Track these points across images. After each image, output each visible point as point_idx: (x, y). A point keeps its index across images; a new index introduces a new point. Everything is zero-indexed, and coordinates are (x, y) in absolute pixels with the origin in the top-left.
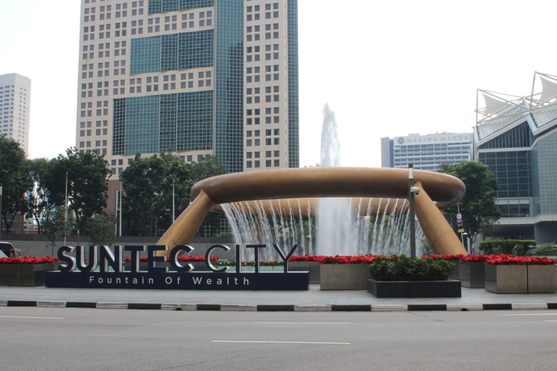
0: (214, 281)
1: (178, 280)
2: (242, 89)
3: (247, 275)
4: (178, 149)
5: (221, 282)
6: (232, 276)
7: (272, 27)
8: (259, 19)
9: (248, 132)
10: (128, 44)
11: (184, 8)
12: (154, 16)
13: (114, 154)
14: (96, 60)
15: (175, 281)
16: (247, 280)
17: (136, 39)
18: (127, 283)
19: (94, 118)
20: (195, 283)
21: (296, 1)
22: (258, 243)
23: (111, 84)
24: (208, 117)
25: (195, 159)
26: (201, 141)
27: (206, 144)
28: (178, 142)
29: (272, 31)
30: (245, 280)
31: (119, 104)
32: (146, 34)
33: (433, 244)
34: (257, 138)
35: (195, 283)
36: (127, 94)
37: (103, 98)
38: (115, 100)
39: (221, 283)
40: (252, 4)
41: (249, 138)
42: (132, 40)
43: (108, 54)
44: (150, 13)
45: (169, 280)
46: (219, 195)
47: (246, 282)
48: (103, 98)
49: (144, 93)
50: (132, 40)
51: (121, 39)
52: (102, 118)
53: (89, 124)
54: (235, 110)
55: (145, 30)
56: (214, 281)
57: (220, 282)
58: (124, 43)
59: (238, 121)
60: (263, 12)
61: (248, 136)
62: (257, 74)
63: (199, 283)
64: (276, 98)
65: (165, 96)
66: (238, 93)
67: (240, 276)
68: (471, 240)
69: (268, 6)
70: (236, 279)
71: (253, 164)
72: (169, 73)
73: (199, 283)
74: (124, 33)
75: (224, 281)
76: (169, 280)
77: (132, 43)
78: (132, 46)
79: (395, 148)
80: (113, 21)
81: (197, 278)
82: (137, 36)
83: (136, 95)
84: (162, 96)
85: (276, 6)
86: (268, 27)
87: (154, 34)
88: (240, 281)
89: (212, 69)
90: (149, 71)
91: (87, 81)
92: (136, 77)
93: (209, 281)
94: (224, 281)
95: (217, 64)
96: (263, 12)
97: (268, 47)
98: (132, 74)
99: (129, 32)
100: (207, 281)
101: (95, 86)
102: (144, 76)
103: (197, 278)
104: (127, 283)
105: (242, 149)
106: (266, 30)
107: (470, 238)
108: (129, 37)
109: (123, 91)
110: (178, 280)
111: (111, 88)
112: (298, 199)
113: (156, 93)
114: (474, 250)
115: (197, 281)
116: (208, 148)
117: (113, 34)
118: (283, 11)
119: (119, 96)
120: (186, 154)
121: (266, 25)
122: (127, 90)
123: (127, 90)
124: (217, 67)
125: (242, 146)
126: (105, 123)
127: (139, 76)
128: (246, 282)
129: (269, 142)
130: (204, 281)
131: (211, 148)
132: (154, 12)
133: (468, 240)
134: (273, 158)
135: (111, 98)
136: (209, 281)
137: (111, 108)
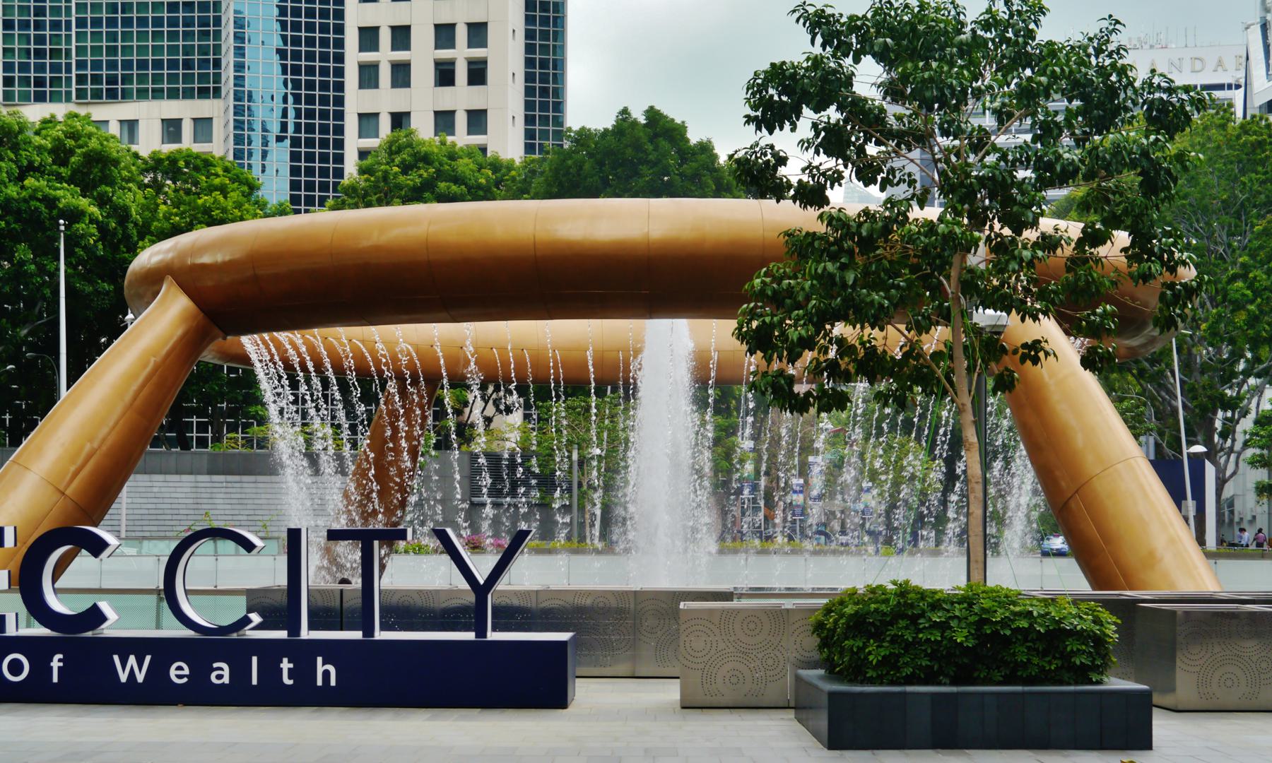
0: (200, 671)
1: (56, 663)
2: (340, 116)
3: (331, 650)
4: (81, 94)
5: (226, 673)
6: (271, 652)
9: (362, 30)
15: (41, 668)
16: (332, 669)
18: (287, 681)
20: (123, 677)
21: (560, 8)
22: (379, 523)
24: (204, 50)
26: (173, 64)
28: (81, 65)
30: (320, 669)
33: (1066, 503)
34: (401, 55)
35: (123, 677)
39: (226, 680)
40: (383, 16)
41: (369, 57)
45: (16, 667)
46: (233, 301)
47: (326, 674)
54: (310, 42)
56: (200, 671)
57: (222, 673)
59: (324, 143)
60: (423, 55)
61: (362, 48)
62: (401, 55)
63: (140, 678)
66: (324, 130)
67: (304, 654)
68: (1220, 472)
69: (444, 34)
70: (286, 665)
71: (385, 74)
73: (140, 678)
75: (240, 672)
76: (16, 667)
81: (132, 660)
85: (478, 32)
88: (304, 671)
93: (178, 672)
94: (240, 672)
96: (423, 55)
100: (173, 672)
103: (132, 660)
104: (287, 681)
105: (340, 101)
107: (1215, 463)
110: (56, 663)
112: (373, 328)
114: (1231, 504)
115: (132, 669)
116: (203, 93)
118: (507, 55)
120: (112, 114)
121: (438, 27)
125: (340, 87)
128: (326, 674)
129: (445, 75)
130: (158, 672)
131: (217, 93)
133: (1210, 471)
134: (461, 53)
136: (178, 672)
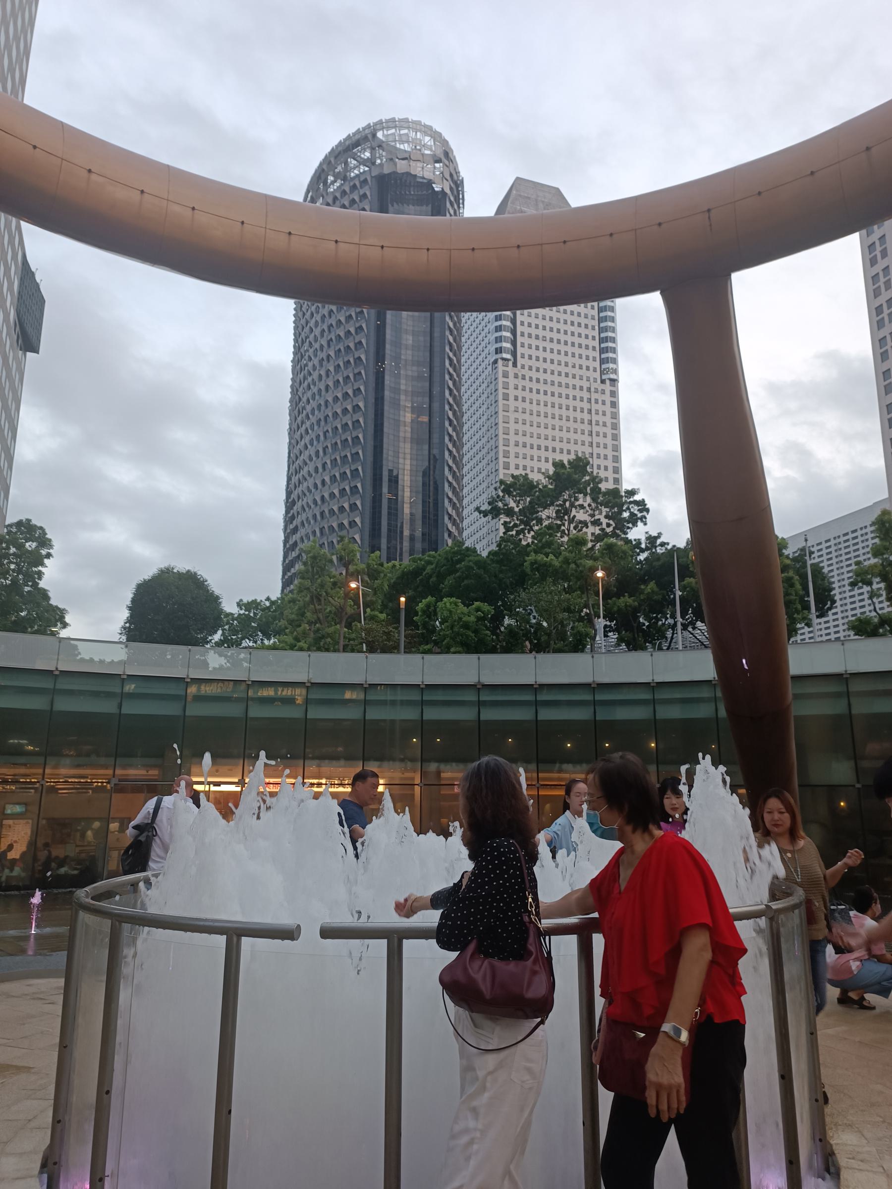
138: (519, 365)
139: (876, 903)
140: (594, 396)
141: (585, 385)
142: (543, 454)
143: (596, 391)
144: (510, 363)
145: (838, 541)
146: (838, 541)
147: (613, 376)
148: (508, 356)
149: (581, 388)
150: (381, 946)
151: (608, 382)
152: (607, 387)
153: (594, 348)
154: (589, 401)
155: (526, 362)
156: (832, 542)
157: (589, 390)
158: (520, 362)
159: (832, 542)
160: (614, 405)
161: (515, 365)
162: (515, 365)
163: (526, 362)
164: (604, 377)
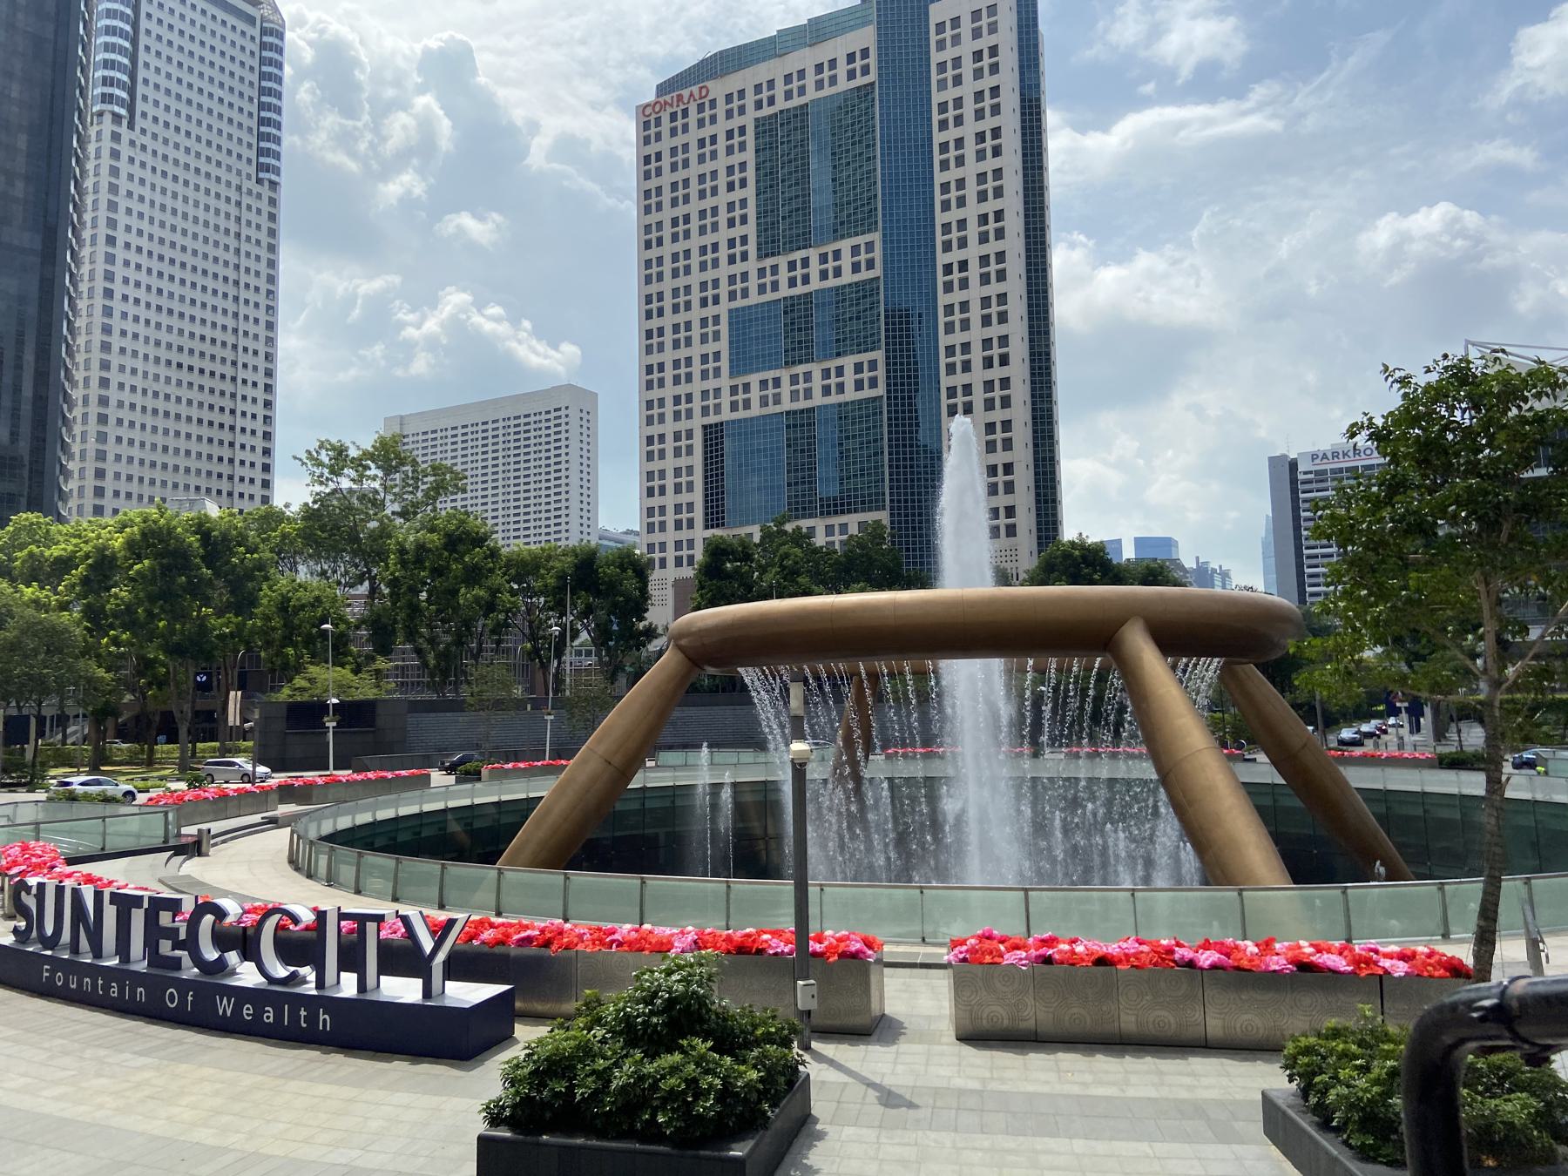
7: (997, 385)
8: (960, 83)
10: (724, 320)
11: (829, 513)
12: (769, 262)
13: (707, 527)
14: (668, 285)
17: (737, 310)
19: (670, 463)
23: (697, 397)
25: (853, 530)
27: (874, 504)
29: (997, 393)
31: (713, 434)
32: (754, 299)
36: (726, 415)
37: (683, 425)
38: (705, 427)
42: (730, 311)
43: (688, 305)
44: (760, 257)
48: (683, 425)
49: (756, 410)
50: (730, 311)
51: (710, 311)
52: (683, 462)
53: (662, 510)
55: (753, 290)
58: (716, 319)
64: (1004, 360)
65: (795, 412)
72: (800, 369)
74: (716, 300)
77: (730, 318)
78: (730, 324)
79: (1301, 477)
80: (695, 278)
82: (740, 303)
83: (741, 414)
84: (788, 413)
85: (992, 10)
86: (989, 385)
87: (770, 296)
89: (876, 237)
90: (764, 369)
91: (654, 359)
92: (740, 381)
95: (887, 344)
97: (987, 343)
98: (732, 375)
99: (724, 297)
101: (669, 402)
102: (754, 379)
106: (967, 279)
108: (723, 308)
109: (718, 408)
111: (697, 405)
113: (778, 409)
117: (696, 304)
118: (1007, 20)
119: (712, 419)
122: (726, 407)
123: (726, 407)
124: (887, 351)
126: (690, 506)
127: (746, 379)
132: (767, 255)
135: (697, 423)
137: (698, 441)
138: (137, 128)
139: (803, 1063)
140: (246, 200)
141: (235, 181)
142: (146, 140)
143: (250, 192)
144: (125, 122)
145: (507, 423)
146: (507, 423)
147: (273, 177)
148: (123, 112)
149: (227, 231)
150: (1128, 894)
151: (266, 183)
152: (265, 191)
153: (250, 145)
154: (236, 299)
155: (148, 124)
156: (501, 424)
157: (239, 188)
158: (140, 122)
159: (501, 424)
160: (272, 279)
161: (131, 126)
162: (131, 126)
163: (148, 124)
164: (261, 175)
